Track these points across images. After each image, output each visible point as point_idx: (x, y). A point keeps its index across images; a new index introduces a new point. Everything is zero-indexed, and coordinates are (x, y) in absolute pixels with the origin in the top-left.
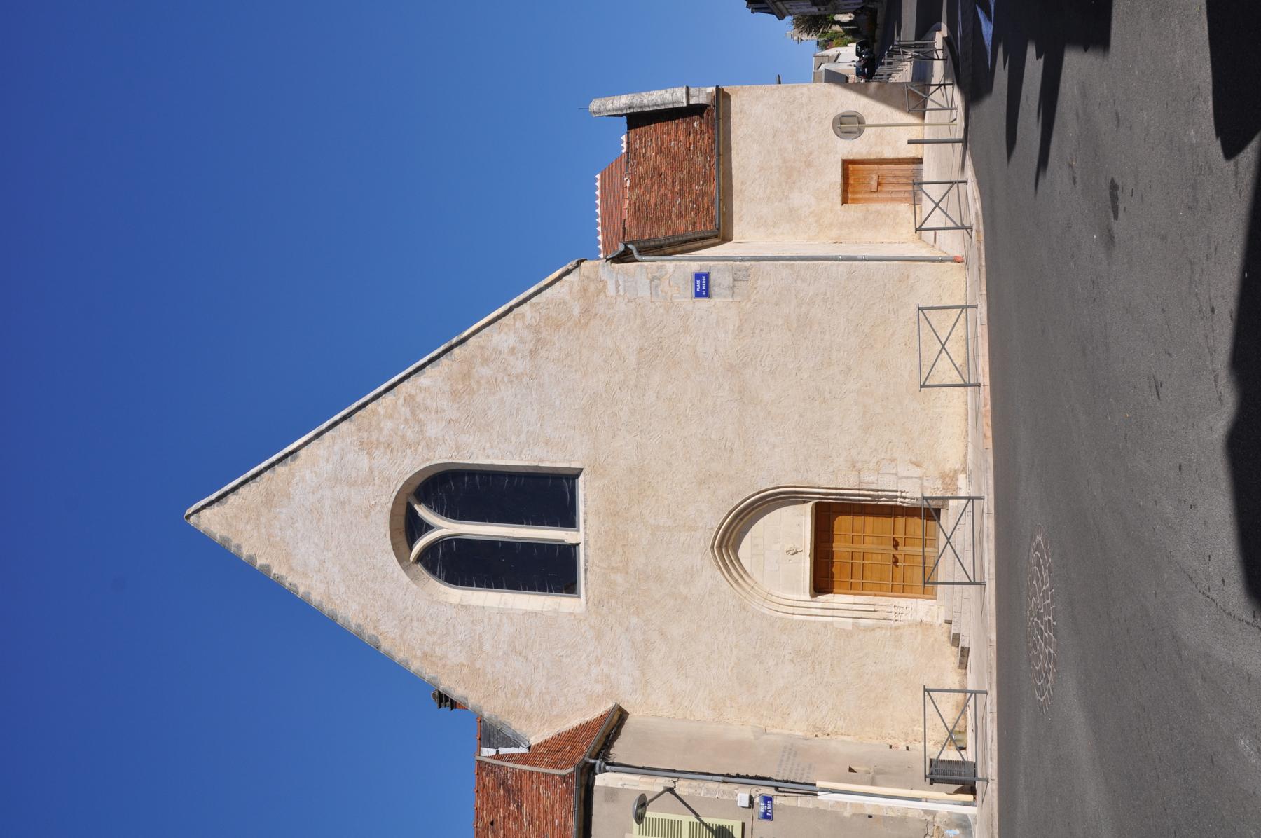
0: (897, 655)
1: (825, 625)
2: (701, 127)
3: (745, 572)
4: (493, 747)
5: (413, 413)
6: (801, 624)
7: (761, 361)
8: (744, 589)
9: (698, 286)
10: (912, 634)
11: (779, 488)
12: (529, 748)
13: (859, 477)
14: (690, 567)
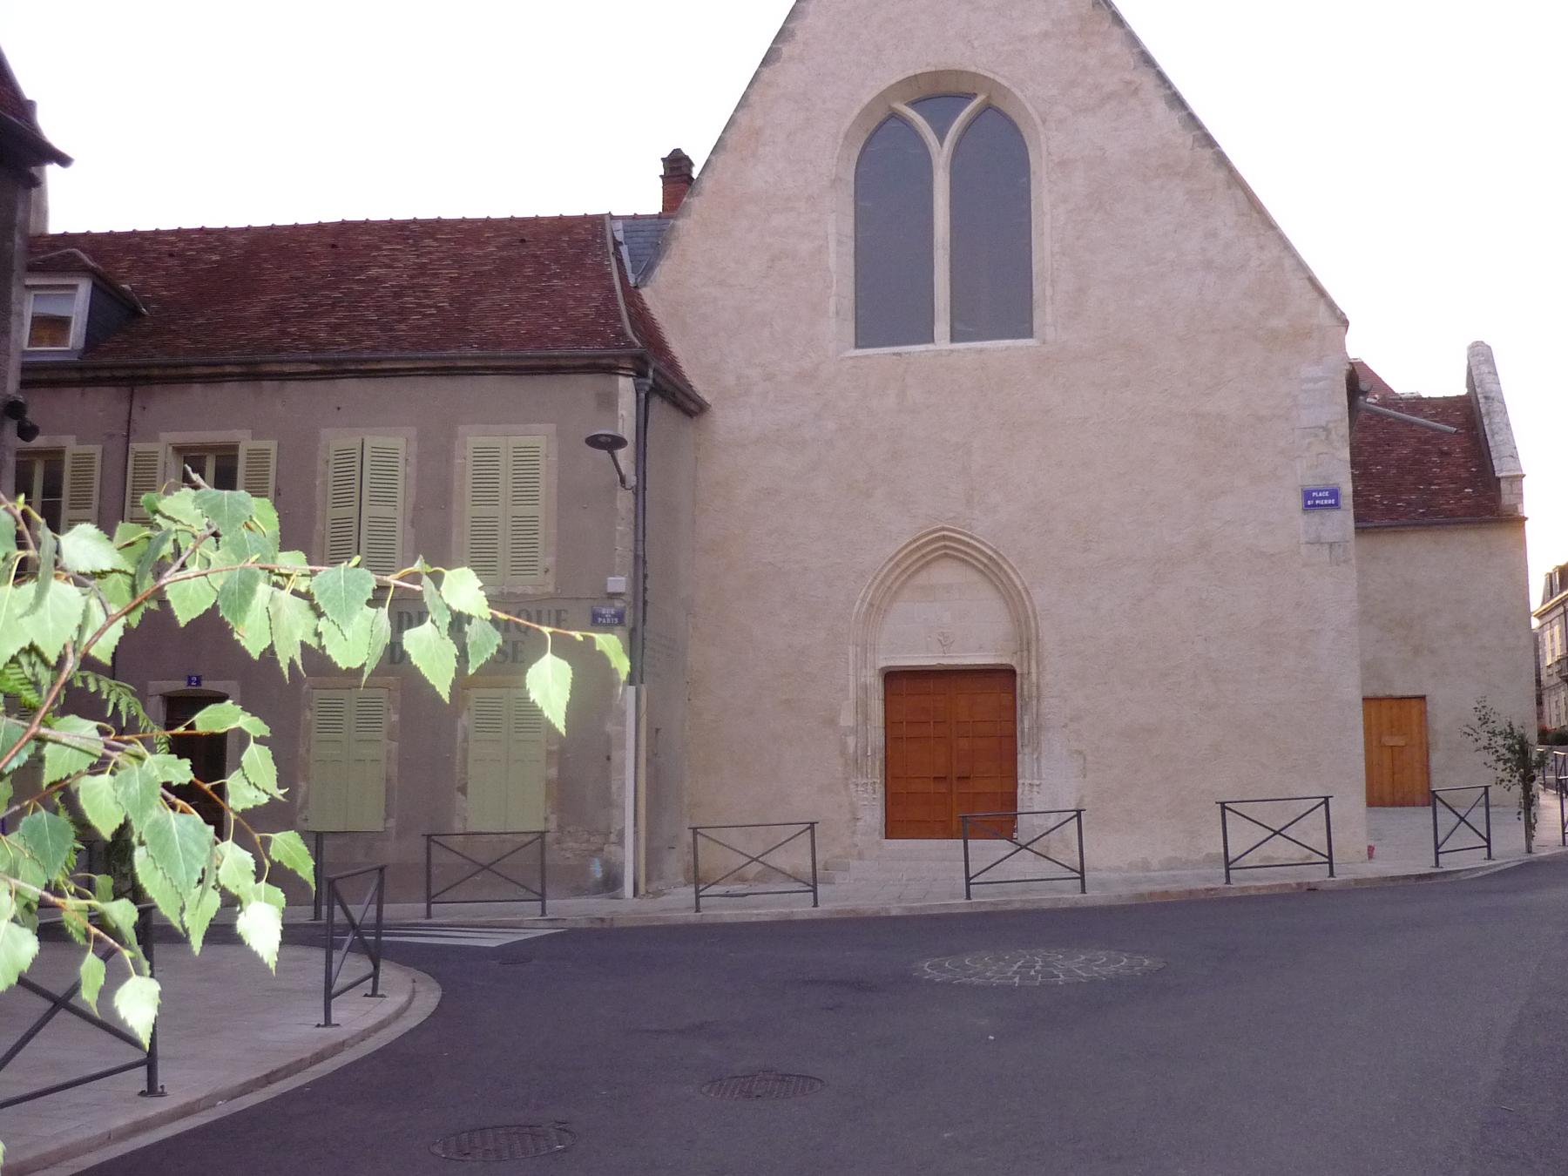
2: (1465, 498)
4: (625, 237)
5: (1110, 96)
7: (1216, 585)
9: (1320, 495)
12: (636, 287)
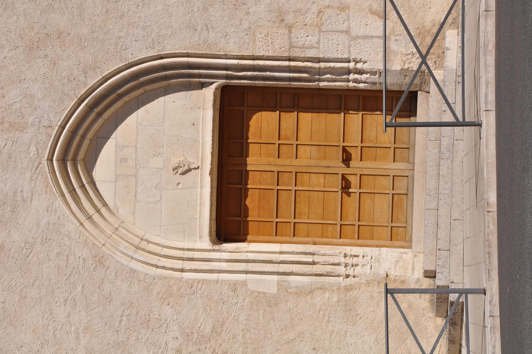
0: (349, 334)
1: (234, 287)
3: (105, 205)
6: (195, 285)
8: (102, 231)
10: (372, 297)
11: (161, 57)
13: (290, 37)
14: (10, 194)
